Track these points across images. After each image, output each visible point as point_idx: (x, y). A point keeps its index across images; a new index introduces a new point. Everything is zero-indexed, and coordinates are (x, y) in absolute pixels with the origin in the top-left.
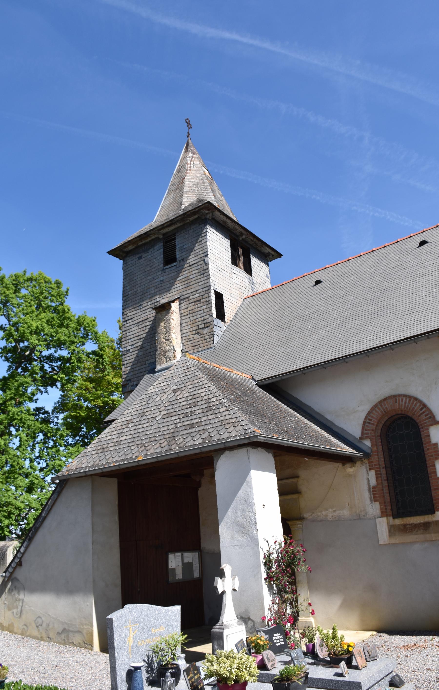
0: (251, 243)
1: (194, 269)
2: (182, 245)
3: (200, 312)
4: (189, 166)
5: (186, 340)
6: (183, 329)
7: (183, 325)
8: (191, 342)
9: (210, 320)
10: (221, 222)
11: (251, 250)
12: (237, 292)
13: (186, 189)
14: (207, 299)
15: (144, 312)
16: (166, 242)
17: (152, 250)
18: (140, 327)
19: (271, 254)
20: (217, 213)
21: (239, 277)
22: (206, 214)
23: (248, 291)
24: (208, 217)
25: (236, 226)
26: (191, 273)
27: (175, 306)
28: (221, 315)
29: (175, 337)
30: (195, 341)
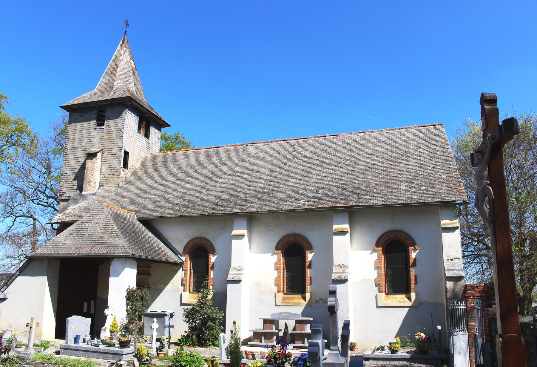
9: (119, 168)
13: (118, 76)
27: (99, 155)
28: (125, 166)
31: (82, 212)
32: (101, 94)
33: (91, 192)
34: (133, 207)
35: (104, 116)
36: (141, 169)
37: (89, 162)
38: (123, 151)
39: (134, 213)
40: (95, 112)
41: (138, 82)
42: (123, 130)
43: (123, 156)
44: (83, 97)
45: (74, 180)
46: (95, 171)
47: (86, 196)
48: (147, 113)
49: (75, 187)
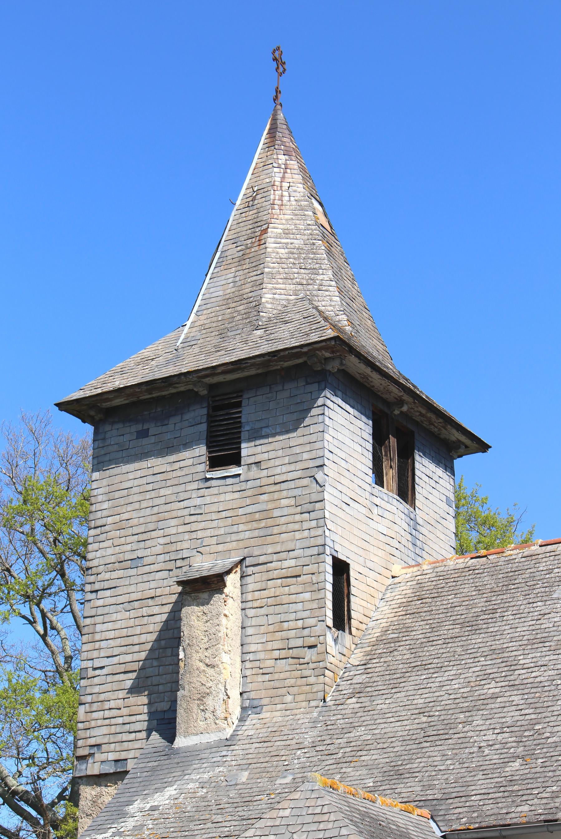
0: (418, 419)
1: (284, 494)
2: (258, 426)
3: (293, 607)
4: (278, 193)
5: (255, 671)
6: (248, 640)
7: (250, 631)
8: (267, 677)
10: (358, 377)
11: (417, 436)
12: (380, 553)
13: (270, 266)
14: (314, 577)
15: (146, 578)
16: (216, 409)
17: (177, 419)
18: (133, 614)
19: (463, 443)
20: (353, 359)
21: (386, 514)
22: (326, 359)
23: (403, 549)
24: (329, 367)
25: (391, 386)
26: (277, 504)
28: (341, 619)
29: (229, 662)
30: (276, 676)
31: (191, 819)
32: (216, 341)
33: (212, 738)
34: (412, 788)
35: (238, 424)
36: (408, 630)
37: (192, 615)
38: (329, 560)
39: (426, 812)
40: (199, 412)
41: (348, 284)
42: (319, 476)
43: (330, 578)
44: (147, 360)
45: (134, 690)
46: (222, 649)
47: (193, 754)
48: (400, 402)
49: (142, 720)
